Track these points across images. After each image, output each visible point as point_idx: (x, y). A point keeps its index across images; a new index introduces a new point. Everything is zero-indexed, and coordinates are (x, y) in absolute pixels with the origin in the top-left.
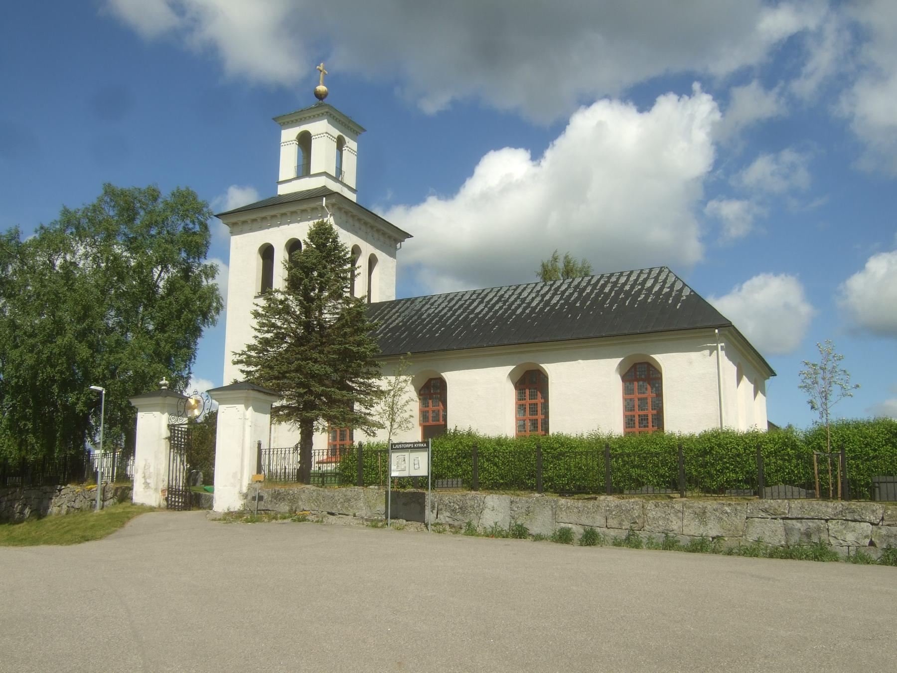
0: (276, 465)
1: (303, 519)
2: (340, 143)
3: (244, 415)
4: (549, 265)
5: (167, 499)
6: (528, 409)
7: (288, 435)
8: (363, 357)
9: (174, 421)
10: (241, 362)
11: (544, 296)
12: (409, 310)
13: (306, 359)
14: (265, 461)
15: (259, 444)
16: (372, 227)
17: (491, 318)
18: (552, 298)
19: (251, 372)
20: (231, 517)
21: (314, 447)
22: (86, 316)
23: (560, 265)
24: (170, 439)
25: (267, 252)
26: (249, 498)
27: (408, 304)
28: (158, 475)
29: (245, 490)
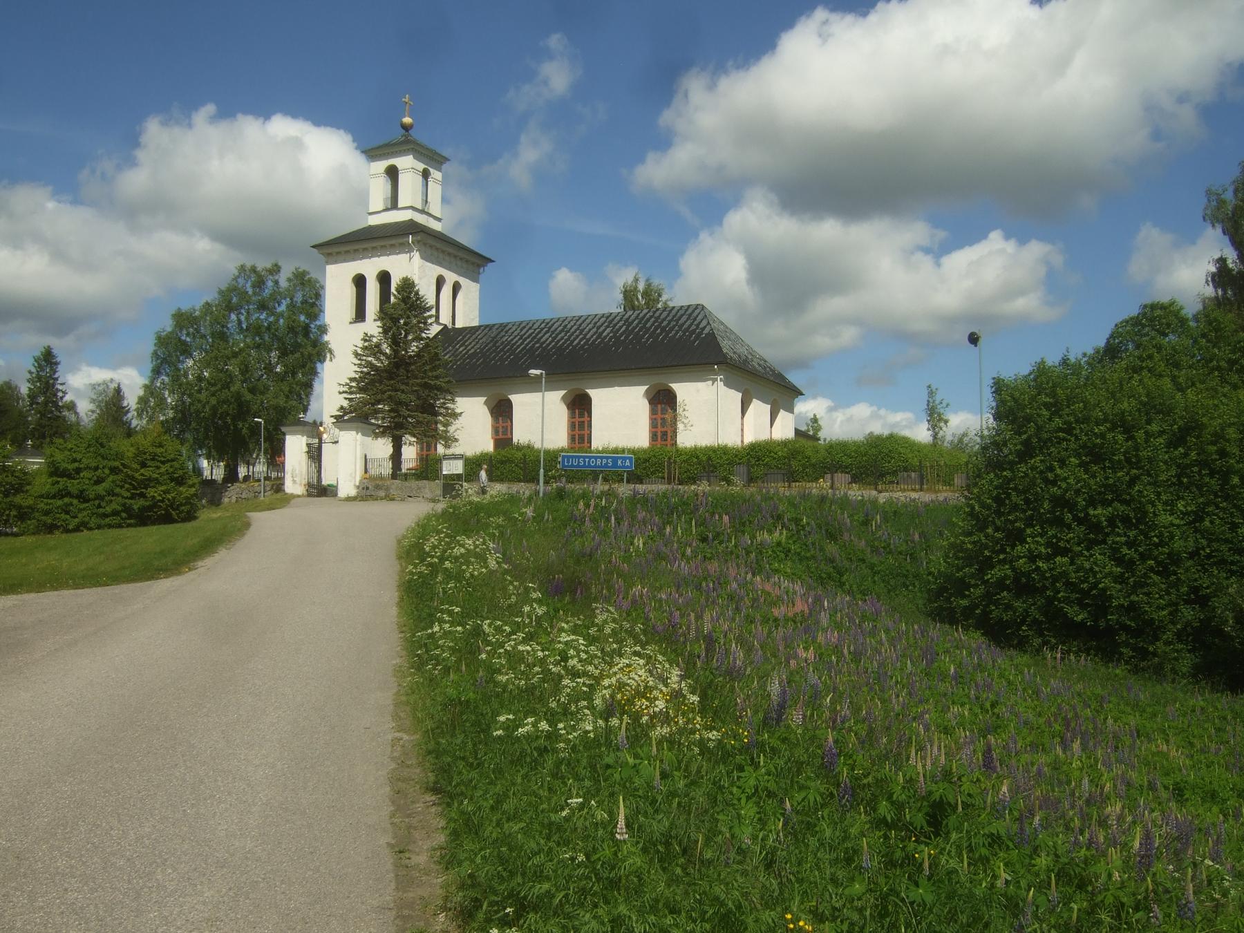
0: (373, 471)
1: (393, 500)
2: (426, 175)
7: (382, 448)
8: (439, 389)
9: (310, 441)
14: (370, 466)
16: (455, 257)
20: (349, 499)
22: (247, 371)
25: (360, 282)
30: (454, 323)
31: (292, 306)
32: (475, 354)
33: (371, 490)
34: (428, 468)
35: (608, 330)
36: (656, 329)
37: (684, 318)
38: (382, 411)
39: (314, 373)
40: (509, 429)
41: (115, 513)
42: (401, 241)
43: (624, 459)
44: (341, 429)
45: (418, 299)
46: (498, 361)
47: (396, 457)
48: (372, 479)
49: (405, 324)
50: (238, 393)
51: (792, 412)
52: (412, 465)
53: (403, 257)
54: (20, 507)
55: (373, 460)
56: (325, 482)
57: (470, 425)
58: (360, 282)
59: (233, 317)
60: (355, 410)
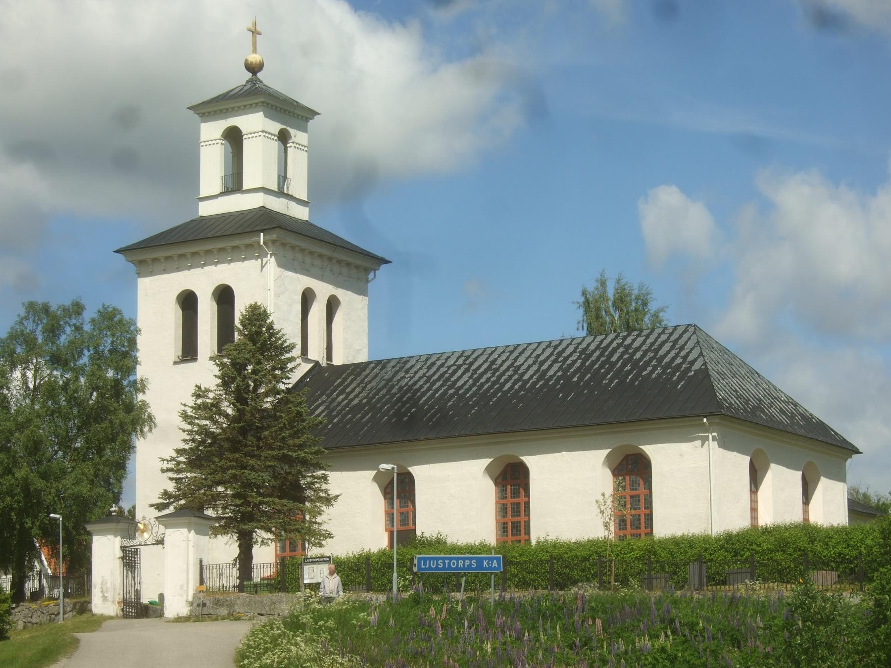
0: (212, 582)
1: (238, 619)
2: (283, 137)
3: (188, 537)
4: (324, 486)
5: (123, 610)
6: (509, 510)
7: (225, 549)
8: (304, 462)
10: (168, 470)
11: (542, 363)
12: (378, 379)
13: (243, 467)
14: (207, 574)
15: (201, 561)
16: (330, 259)
17: (472, 396)
18: (550, 367)
19: (181, 479)
20: (179, 620)
21: (254, 561)
23: (611, 293)
24: (123, 558)
25: (188, 301)
26: (195, 605)
27: (377, 370)
28: (115, 589)
29: (190, 599)
30: (329, 357)
31: (98, 356)
32: (360, 406)
33: (208, 607)
34: (287, 578)
35: (556, 367)
36: (624, 365)
37: (667, 346)
38: (219, 496)
39: (128, 448)
42: (247, 241)
43: (491, 559)
44: (167, 527)
45: (272, 335)
46: (403, 415)
47: (245, 559)
48: (209, 592)
49: (254, 372)
50: (25, 479)
52: (269, 572)
53: (251, 265)
55: (212, 567)
57: (352, 511)
58: (188, 301)
60: (184, 496)
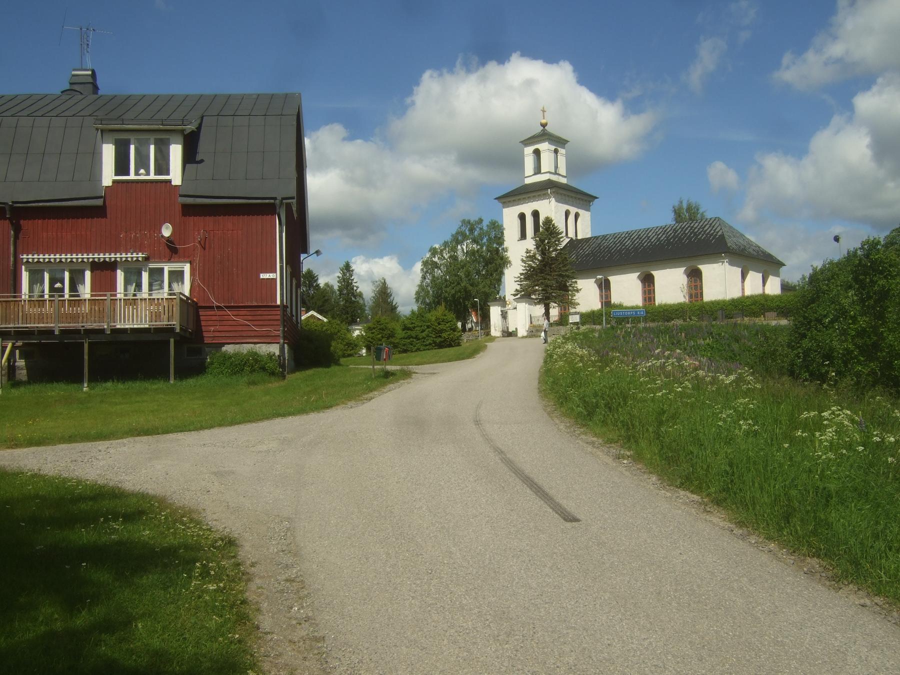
0: (535, 323)
2: (556, 151)
7: (539, 310)
8: (568, 276)
20: (523, 337)
25: (522, 217)
30: (576, 236)
31: (490, 239)
33: (534, 332)
39: (502, 273)
40: (608, 296)
41: (430, 344)
46: (601, 258)
47: (547, 314)
48: (534, 326)
51: (779, 276)
52: (556, 318)
54: (394, 343)
56: (510, 330)
57: (586, 295)
58: (522, 217)
59: (459, 247)
